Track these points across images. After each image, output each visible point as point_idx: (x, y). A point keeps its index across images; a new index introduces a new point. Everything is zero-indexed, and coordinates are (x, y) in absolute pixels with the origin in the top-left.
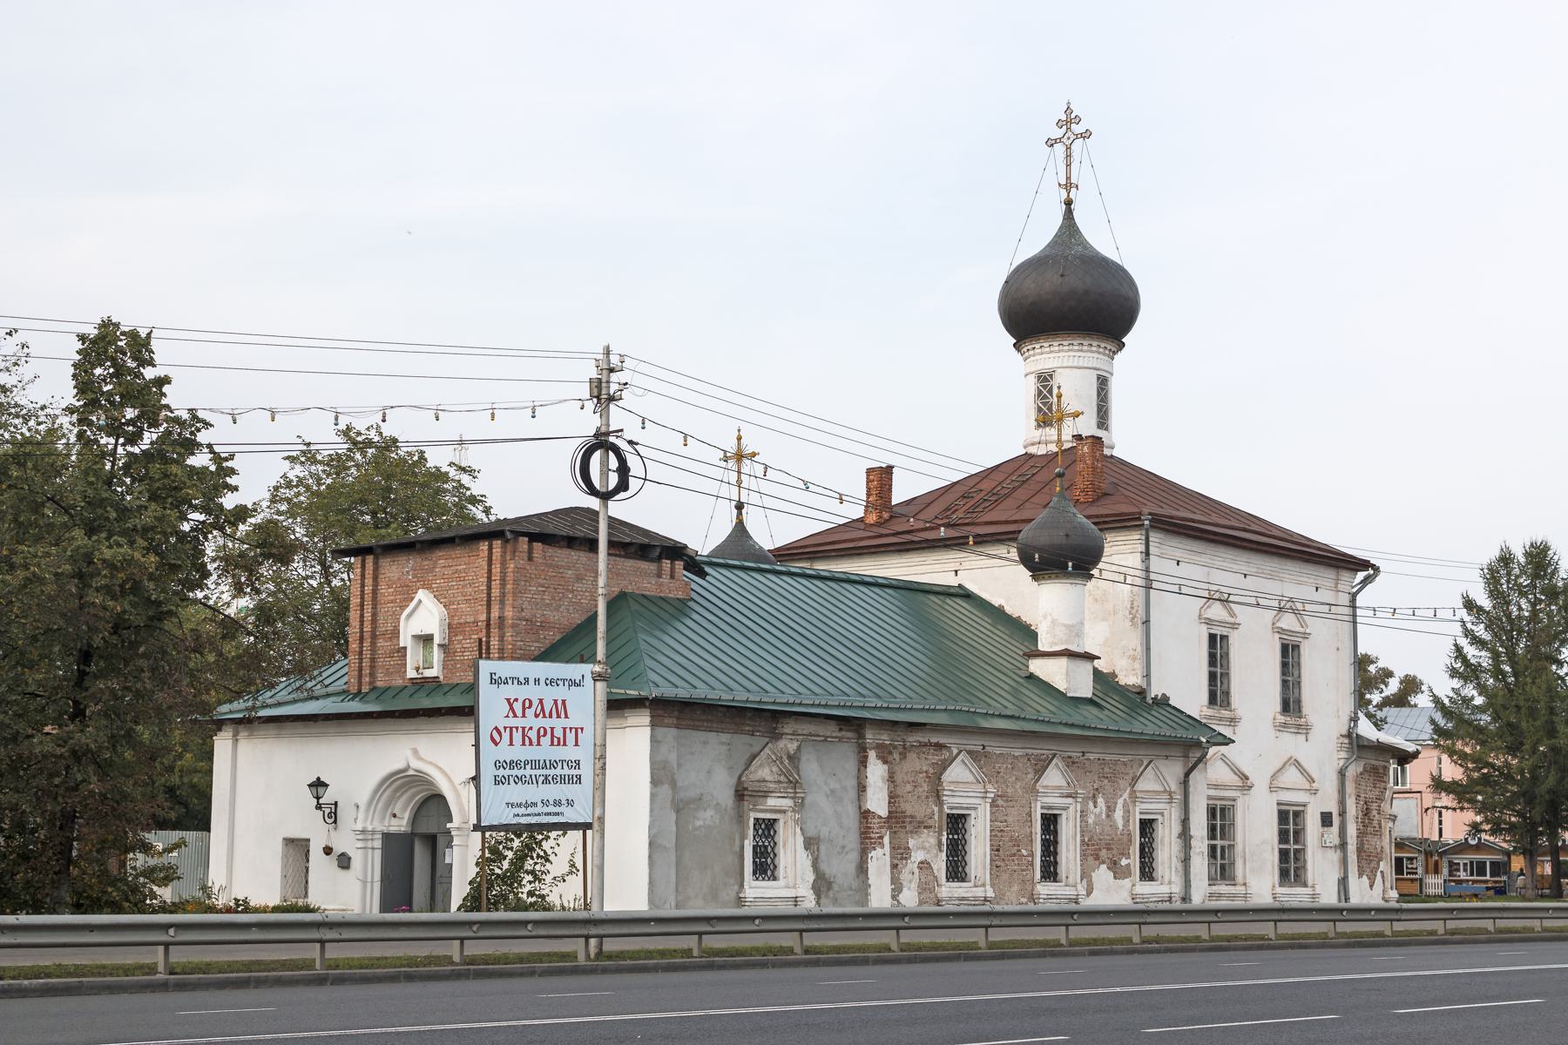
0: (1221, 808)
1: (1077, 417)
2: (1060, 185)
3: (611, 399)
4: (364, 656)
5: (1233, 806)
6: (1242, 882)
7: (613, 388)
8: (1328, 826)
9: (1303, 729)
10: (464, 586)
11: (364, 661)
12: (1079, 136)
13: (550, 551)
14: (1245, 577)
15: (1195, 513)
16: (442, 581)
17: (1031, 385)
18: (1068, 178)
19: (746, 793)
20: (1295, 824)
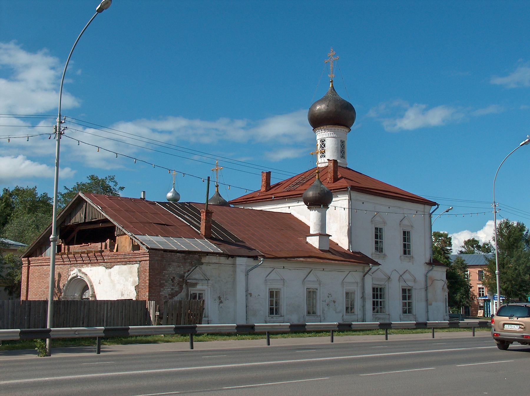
0: (380, 288)
6: (388, 314)
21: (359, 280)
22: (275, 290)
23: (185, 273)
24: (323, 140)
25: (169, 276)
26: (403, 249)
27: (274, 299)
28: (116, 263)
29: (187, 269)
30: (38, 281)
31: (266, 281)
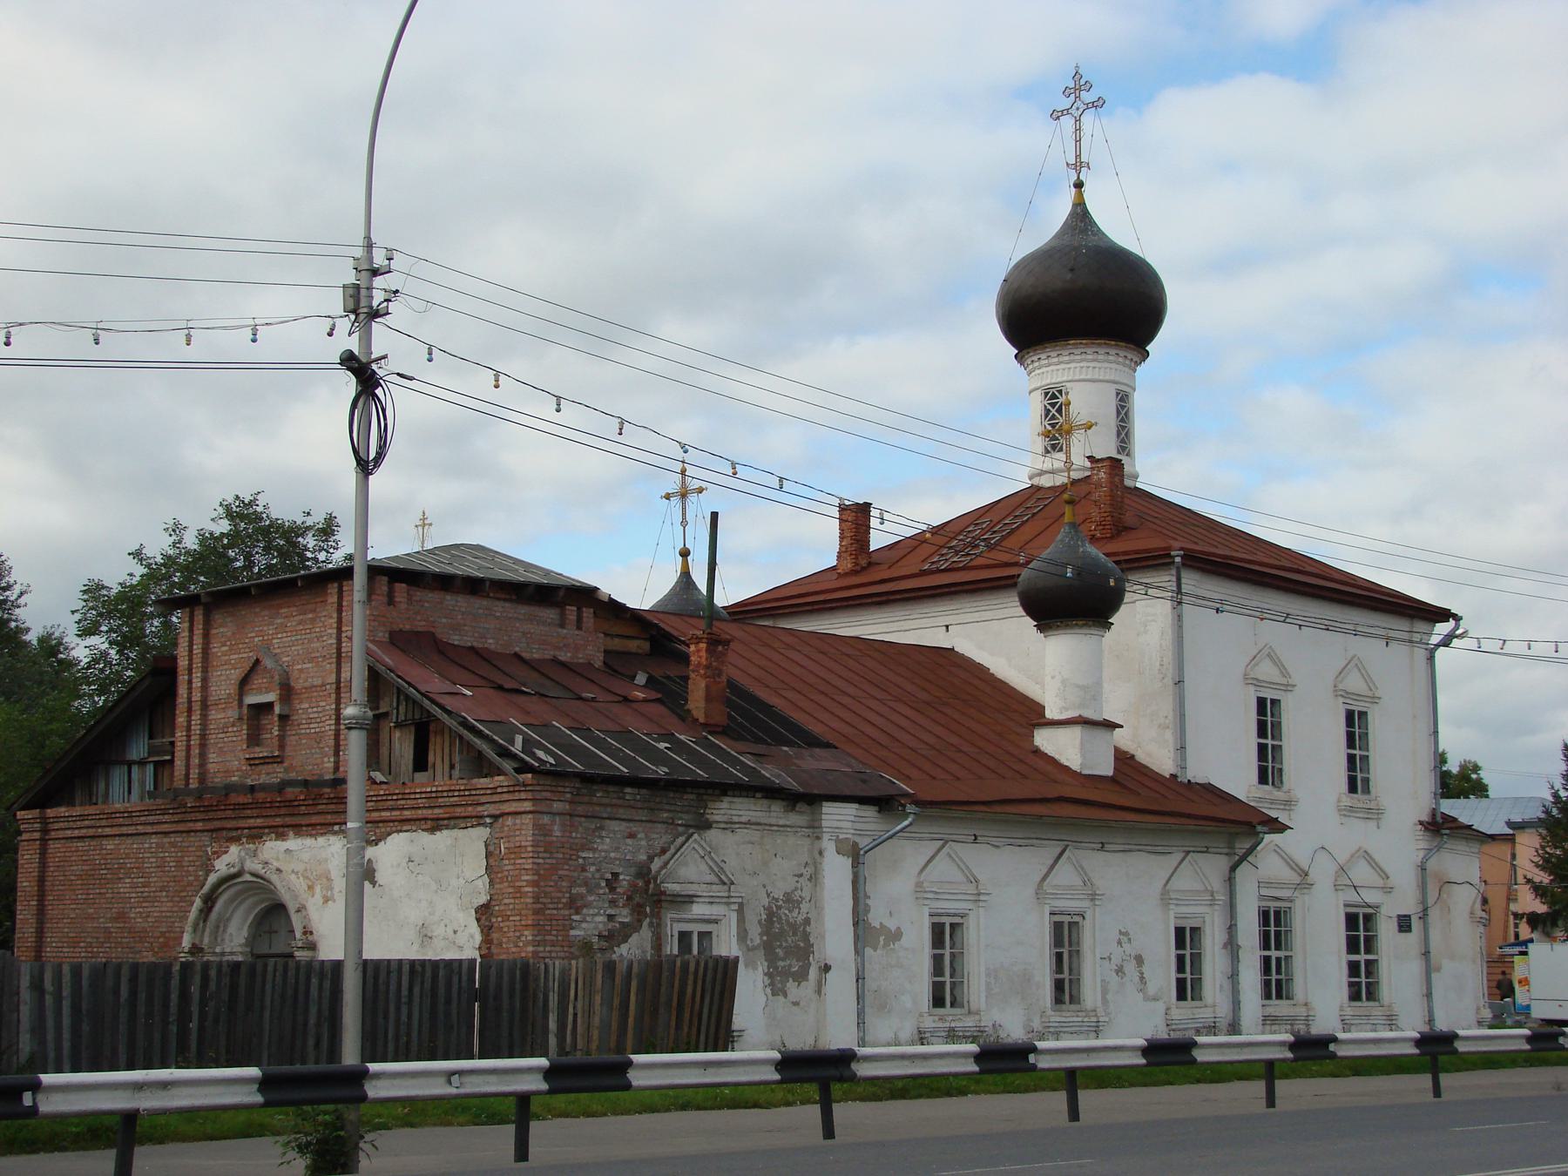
0: (1275, 911)
1: (1089, 429)
2: (1067, 164)
3: (375, 314)
4: (193, 732)
5: (1290, 908)
7: (378, 297)
8: (1406, 931)
9: (1374, 814)
10: (310, 641)
11: (193, 738)
12: (1090, 105)
13: (419, 594)
14: (1300, 629)
15: (1237, 551)
16: (285, 635)
17: (1037, 403)
18: (1078, 156)
19: (663, 898)
20: (1366, 930)
21: (1217, 883)
22: (947, 921)
23: (651, 859)
24: (1054, 390)
25: (598, 870)
26: (1347, 773)
27: (947, 952)
28: (396, 823)
29: (658, 844)
30: (81, 892)
31: (921, 887)
